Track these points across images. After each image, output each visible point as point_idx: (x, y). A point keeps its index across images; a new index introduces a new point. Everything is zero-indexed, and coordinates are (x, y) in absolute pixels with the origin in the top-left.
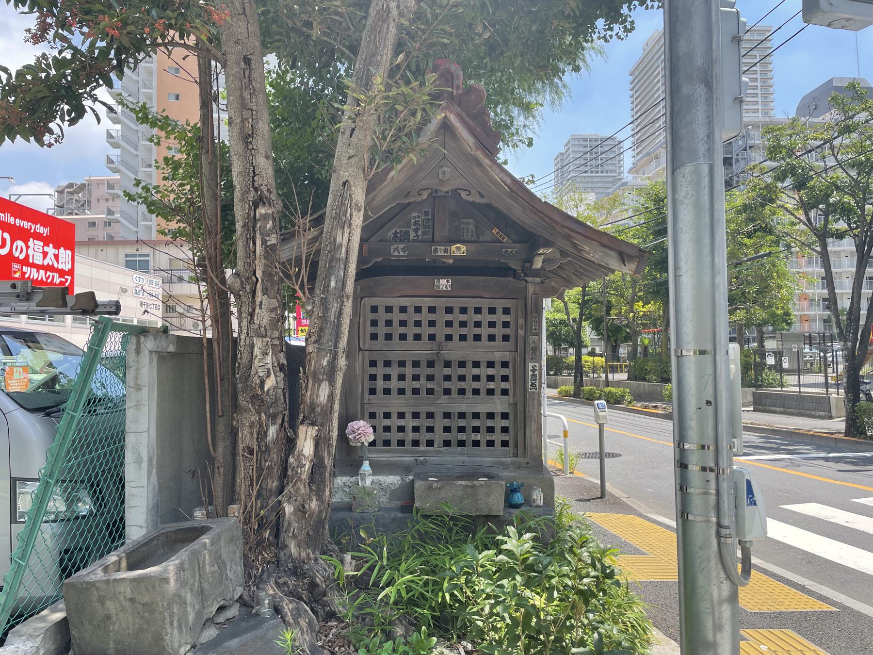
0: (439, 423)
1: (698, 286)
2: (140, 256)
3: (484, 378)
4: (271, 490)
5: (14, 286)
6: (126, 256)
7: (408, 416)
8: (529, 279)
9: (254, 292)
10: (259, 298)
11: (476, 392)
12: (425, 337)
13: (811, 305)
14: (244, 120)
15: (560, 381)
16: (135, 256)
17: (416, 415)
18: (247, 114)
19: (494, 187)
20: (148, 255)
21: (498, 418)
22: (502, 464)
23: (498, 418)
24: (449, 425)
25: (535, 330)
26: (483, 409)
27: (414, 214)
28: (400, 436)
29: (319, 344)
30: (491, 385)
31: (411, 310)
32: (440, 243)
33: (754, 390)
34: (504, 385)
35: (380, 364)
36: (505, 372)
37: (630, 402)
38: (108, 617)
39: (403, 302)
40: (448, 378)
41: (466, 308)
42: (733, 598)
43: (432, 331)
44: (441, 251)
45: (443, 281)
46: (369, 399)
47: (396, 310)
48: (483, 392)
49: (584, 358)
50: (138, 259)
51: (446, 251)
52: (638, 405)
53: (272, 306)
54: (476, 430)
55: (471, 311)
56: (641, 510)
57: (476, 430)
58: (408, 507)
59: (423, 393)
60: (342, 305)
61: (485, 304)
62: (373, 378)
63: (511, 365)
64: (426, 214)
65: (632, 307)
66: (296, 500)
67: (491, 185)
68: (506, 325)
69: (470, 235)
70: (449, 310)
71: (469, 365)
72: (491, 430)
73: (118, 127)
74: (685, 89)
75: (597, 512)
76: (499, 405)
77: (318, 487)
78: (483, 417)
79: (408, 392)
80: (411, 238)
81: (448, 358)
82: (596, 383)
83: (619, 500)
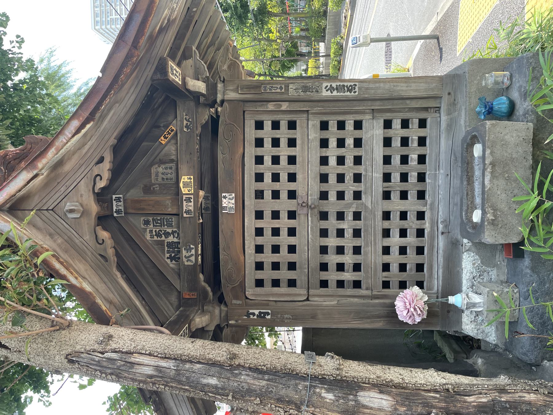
0: (396, 205)
3: (341, 152)
7: (387, 242)
8: (219, 97)
12: (292, 223)
19: (90, 143)
21: (390, 133)
22: (450, 126)
23: (390, 133)
24: (398, 193)
27: (148, 237)
30: (350, 142)
34: (350, 126)
35: (324, 276)
37: (342, 38)
39: (250, 249)
40: (341, 196)
41: (256, 174)
43: (284, 215)
44: (188, 206)
46: (367, 289)
48: (358, 152)
49: (309, 74)
51: (188, 200)
52: (344, 31)
54: (404, 160)
55: (260, 169)
57: (404, 160)
58: (516, 250)
59: (359, 224)
60: (243, 367)
61: (251, 151)
62: (340, 284)
63: (325, 118)
64: (147, 223)
65: (273, 41)
67: (87, 147)
68: (276, 125)
69: (169, 171)
70: (259, 195)
71: (325, 169)
72: (405, 142)
75: (456, 38)
76: (374, 132)
80: (176, 240)
81: (317, 196)
82: (327, 65)
83: (440, 21)
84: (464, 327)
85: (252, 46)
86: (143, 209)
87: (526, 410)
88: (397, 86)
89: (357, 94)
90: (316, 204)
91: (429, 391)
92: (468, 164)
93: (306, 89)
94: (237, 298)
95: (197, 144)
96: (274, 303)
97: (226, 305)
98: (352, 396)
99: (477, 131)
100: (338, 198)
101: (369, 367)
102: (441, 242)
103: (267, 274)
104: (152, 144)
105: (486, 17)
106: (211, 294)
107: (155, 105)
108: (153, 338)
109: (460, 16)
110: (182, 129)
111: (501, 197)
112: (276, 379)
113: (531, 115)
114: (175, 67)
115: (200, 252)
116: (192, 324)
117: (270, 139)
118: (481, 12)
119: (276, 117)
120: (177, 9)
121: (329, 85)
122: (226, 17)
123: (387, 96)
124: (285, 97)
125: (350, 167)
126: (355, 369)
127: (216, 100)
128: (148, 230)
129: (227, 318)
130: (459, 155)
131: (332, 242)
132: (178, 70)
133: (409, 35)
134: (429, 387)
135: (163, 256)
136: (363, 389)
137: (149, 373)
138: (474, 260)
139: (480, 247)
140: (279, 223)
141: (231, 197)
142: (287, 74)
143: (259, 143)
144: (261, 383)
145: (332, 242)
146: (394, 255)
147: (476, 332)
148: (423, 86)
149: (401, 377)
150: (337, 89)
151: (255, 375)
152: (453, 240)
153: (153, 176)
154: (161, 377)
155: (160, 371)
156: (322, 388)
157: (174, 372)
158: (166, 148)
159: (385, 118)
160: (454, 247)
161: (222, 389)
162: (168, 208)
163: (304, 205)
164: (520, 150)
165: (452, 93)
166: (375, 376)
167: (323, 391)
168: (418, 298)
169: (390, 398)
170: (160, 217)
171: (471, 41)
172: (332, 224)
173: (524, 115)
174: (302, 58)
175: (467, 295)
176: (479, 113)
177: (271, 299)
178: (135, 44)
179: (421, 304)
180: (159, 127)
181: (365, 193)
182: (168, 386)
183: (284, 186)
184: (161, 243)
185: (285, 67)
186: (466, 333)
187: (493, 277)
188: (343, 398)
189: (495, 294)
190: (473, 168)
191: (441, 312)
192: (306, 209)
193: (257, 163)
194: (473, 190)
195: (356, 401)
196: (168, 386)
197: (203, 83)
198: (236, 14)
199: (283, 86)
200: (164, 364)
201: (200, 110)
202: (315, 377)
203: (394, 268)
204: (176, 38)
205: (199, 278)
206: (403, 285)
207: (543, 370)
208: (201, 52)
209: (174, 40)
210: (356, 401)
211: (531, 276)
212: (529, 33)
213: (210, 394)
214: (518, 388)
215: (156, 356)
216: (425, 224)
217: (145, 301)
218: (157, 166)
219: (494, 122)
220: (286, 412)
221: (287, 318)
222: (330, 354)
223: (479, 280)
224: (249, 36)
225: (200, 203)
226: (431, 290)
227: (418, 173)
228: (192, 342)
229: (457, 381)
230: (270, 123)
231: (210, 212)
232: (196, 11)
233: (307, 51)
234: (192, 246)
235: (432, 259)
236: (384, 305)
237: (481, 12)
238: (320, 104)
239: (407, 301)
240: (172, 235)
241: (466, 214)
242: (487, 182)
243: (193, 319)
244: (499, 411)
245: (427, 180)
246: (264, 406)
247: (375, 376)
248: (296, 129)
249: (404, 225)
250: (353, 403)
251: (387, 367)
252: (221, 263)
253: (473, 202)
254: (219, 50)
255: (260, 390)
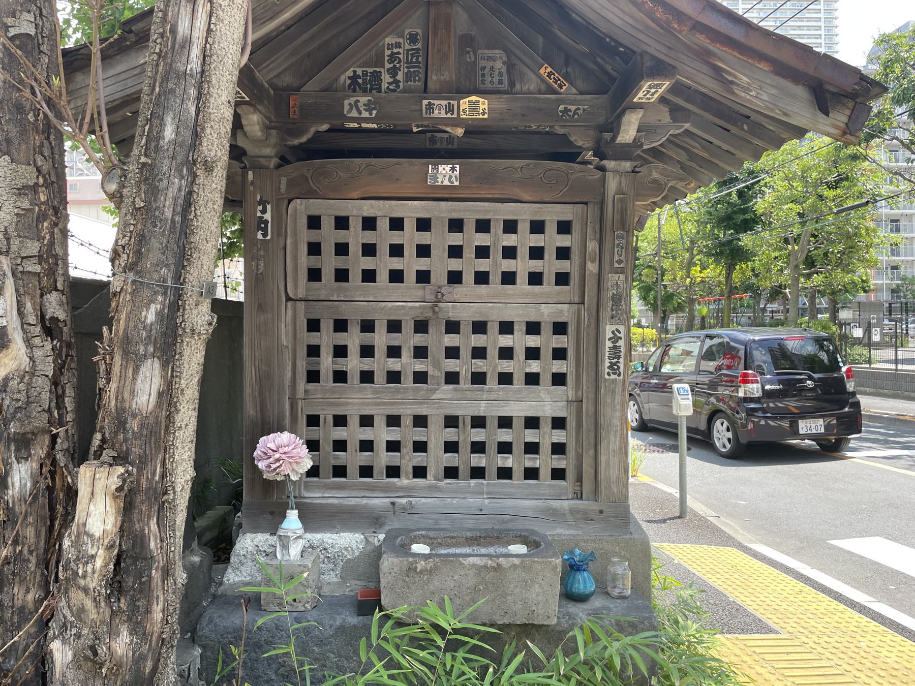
0: (436, 435)
3: (520, 354)
4: (22, 609)
7: (380, 422)
8: (610, 164)
11: (505, 379)
13: (878, 273)
22: (555, 515)
24: (455, 439)
25: (620, 262)
27: (389, 40)
28: (364, 458)
29: (137, 273)
30: (534, 367)
34: (558, 366)
35: (327, 326)
36: (559, 341)
39: (369, 208)
40: (452, 353)
43: (423, 264)
46: (306, 391)
48: (518, 379)
49: (634, 330)
51: (449, 109)
53: (20, 183)
54: (505, 448)
56: (739, 538)
57: (505, 448)
58: (368, 603)
59: (408, 380)
60: (193, 182)
62: (314, 351)
63: (571, 329)
64: (413, 39)
65: (689, 271)
66: (78, 636)
69: (496, 79)
70: (456, 225)
72: (532, 448)
75: (680, 542)
76: (547, 402)
77: (133, 603)
78: (518, 424)
80: (384, 86)
81: (453, 316)
83: (707, 521)
84: (249, 536)
85: (682, 238)
86: (435, 34)
87: (138, 607)
88: (616, 436)
89: (607, 377)
90: (441, 315)
91: (163, 465)
92: (498, 538)
94: (290, 184)
95: (538, 127)
96: (282, 244)
97: (278, 167)
98: (152, 350)
99: (546, 548)
100: (448, 349)
101: (196, 380)
102: (379, 502)
103: (329, 236)
104: (540, 52)
105: (711, 582)
106: (296, 142)
107: (602, 58)
108: (235, 37)
109: (713, 547)
110: (562, 101)
111: (448, 580)
112: (175, 233)
113: (567, 622)
114: (660, 91)
115: (364, 125)
116: (249, 107)
117: (542, 244)
118: (718, 576)
119: (575, 255)
120: (748, 97)
121: (622, 335)
122: (730, 194)
123: (601, 421)
124: (607, 267)
125: (496, 366)
126: (193, 358)
127: (606, 159)
128: (401, 40)
129: (257, 167)
130: (510, 526)
131: (381, 339)
132: (656, 96)
133: (688, 478)
134: (169, 466)
135: (359, 63)
136: (164, 367)
137: (179, 28)
138: (352, 550)
139: (375, 556)
140: (410, 256)
141: (454, 179)
142: (635, 292)
143: (537, 227)
144: (167, 209)
145: (381, 339)
146: (360, 433)
147: (242, 553)
148: (614, 473)
149: (183, 426)
150: (615, 347)
151: (180, 201)
152: (383, 519)
153: (489, 52)
154: (173, 47)
155: (182, 47)
156: (164, 305)
157: (182, 69)
158: (532, 76)
159: (568, 419)
160: (374, 520)
161: (156, 147)
162: (436, 75)
163: (440, 296)
164: (519, 606)
165: (602, 516)
166: (184, 386)
167: (158, 307)
168: (294, 465)
169: (151, 407)
170: (422, 63)
171: (676, 562)
172: (409, 339)
173: (568, 614)
174: (659, 318)
175: (300, 537)
176: (572, 552)
177: (289, 241)
178: (698, 27)
179: (286, 469)
180: (567, 64)
181: (455, 390)
182: (159, 59)
183: (469, 265)
184: (379, 62)
185: (646, 292)
186: (239, 539)
187: (327, 577)
188: (149, 337)
189: (305, 575)
190: (492, 545)
191: (272, 501)
192: (433, 298)
193: (506, 222)
194: (458, 545)
195: (145, 355)
196: (159, 59)
197: (632, 138)
198: (734, 212)
199: (622, 265)
200: (195, 52)
201: (591, 133)
202: (180, 295)
203: (340, 433)
204: (705, 95)
205: (323, 123)
206: (313, 446)
207: (187, 648)
208: (681, 138)
209: (702, 93)
210: (145, 355)
211: (331, 626)
212: (685, 628)
213: (147, 127)
214: (171, 595)
215: (207, 41)
216: (408, 478)
217: (285, 30)
218: (505, 59)
219: (560, 569)
220: (124, 248)
221: (258, 265)
222: (215, 320)
223: (322, 556)
224: (698, 232)
225: (444, 128)
226: (305, 487)
227: (484, 468)
228: (229, 102)
229: (179, 509)
230: (567, 244)
231: (428, 146)
232: (743, 129)
233: (669, 327)
234: (374, 112)
235: (354, 490)
236: (281, 418)
237: (718, 576)
238: (593, 321)
239: (290, 448)
240: (392, 80)
241: (423, 536)
242: (471, 559)
243: (256, 110)
244: (136, 567)
245: (473, 482)
246: (132, 214)
247: (184, 386)
248: (556, 284)
249: (405, 447)
250: (142, 352)
251: (197, 406)
252: (347, 161)
253: (440, 545)
254: (681, 168)
255: (157, 208)
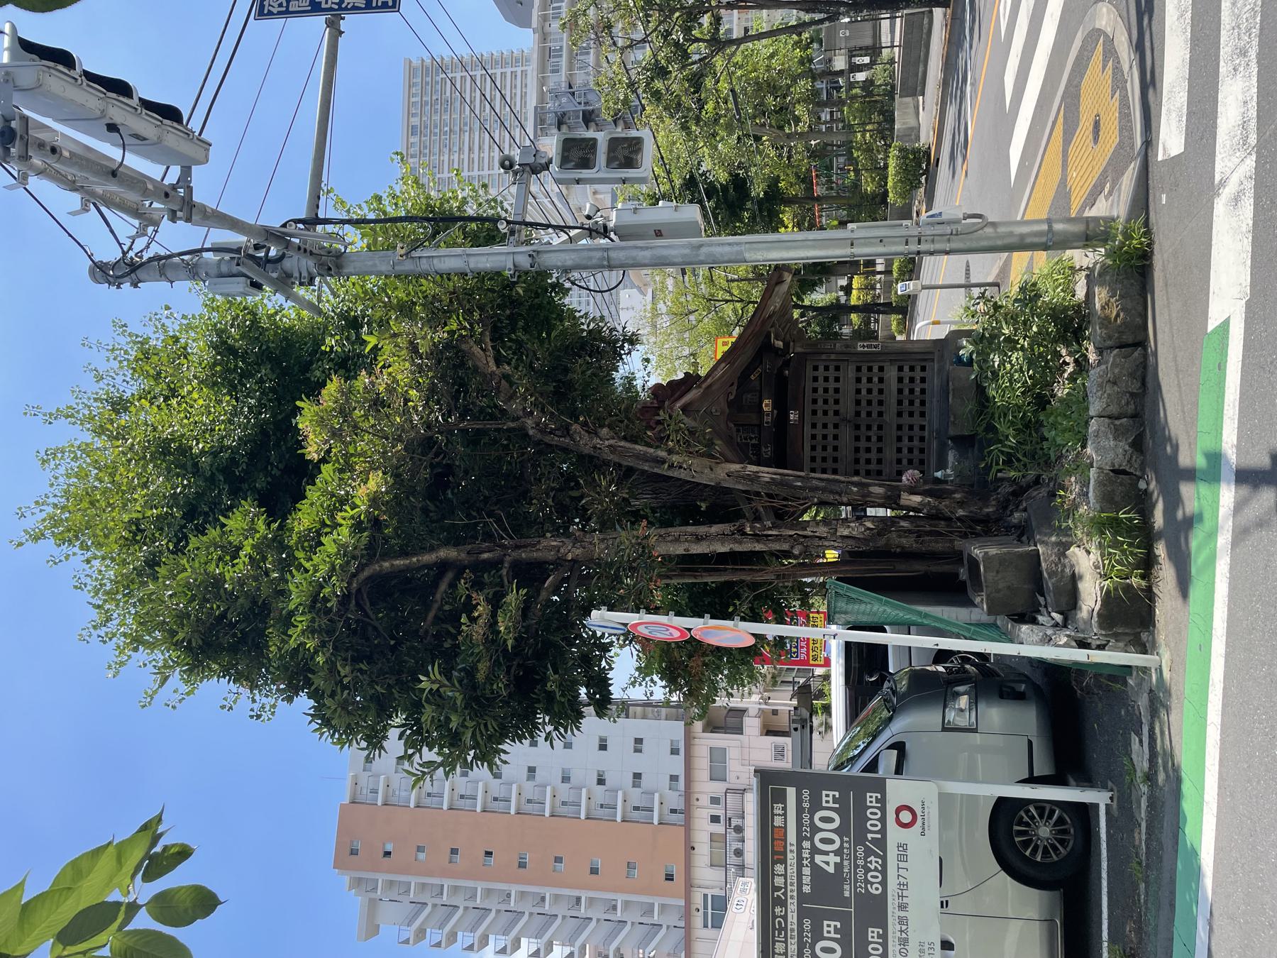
1: (814, 247)
2: (705, 907)
3: (870, 385)
5: (796, 729)
6: (706, 926)
9: (805, 537)
10: (808, 533)
14: (686, 541)
15: (886, 333)
16: (705, 914)
17: (899, 439)
18: (683, 538)
20: (705, 896)
21: (902, 374)
22: (939, 370)
26: (894, 386)
28: (916, 452)
31: (814, 442)
32: (761, 418)
33: (897, 97)
34: (875, 369)
36: (864, 369)
38: (1009, 587)
40: (869, 414)
42: (994, 224)
43: (830, 426)
44: (768, 419)
45: (792, 417)
47: (814, 454)
48: (881, 386)
50: (710, 911)
68: (827, 368)
70: (814, 412)
73: (524, 941)
74: (702, 258)
76: (892, 374)
79: (880, 445)
93: (847, 346)
